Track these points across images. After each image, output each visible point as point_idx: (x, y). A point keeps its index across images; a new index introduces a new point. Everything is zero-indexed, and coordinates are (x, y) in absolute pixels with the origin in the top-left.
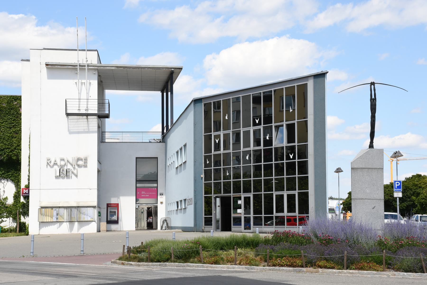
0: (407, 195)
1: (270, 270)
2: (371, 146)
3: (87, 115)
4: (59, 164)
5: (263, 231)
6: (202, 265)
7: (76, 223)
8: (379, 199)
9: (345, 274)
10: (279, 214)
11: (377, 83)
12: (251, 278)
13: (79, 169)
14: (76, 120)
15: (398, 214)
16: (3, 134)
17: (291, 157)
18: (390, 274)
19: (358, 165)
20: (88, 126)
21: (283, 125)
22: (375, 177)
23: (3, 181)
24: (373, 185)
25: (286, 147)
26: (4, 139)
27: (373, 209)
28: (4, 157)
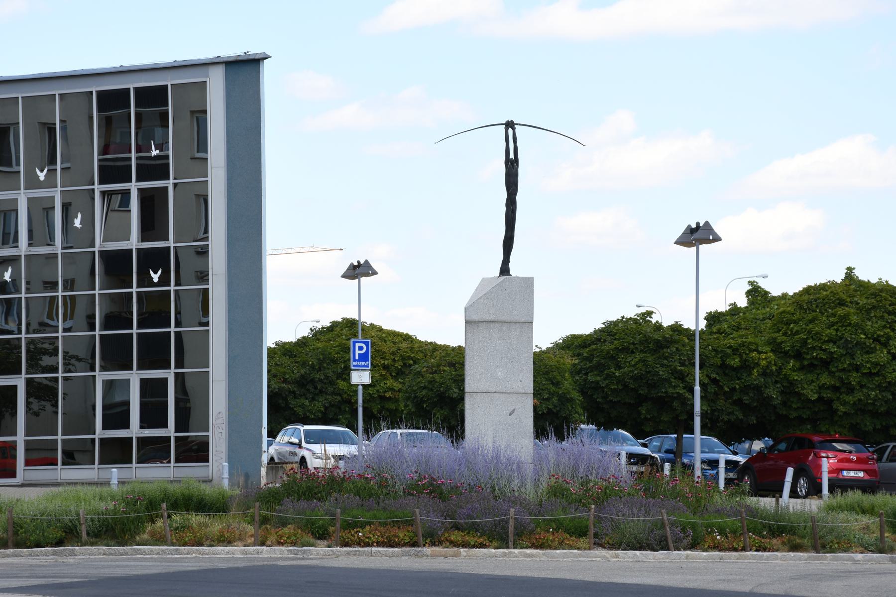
0: (327, 377)
1: (347, 553)
2: (505, 270)
5: (59, 480)
6: (174, 550)
8: (523, 391)
9: (516, 557)
10: (109, 433)
11: (520, 125)
12: (373, 566)
17: (156, 277)
18: (608, 556)
19: (479, 314)
21: (130, 189)
22: (515, 342)
25: (138, 250)
27: (510, 415)
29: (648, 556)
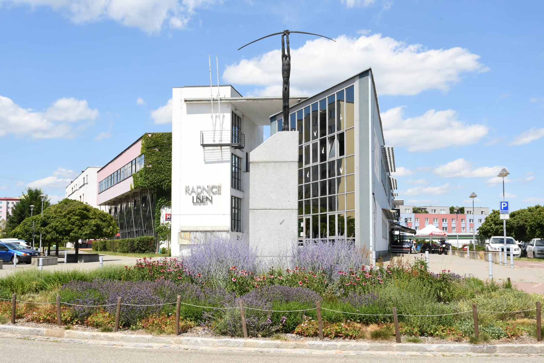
3: (221, 145)
13: (213, 196)
14: (211, 151)
16: (164, 167)
18: (173, 342)
20: (222, 157)
23: (165, 208)
26: (164, 171)
28: (165, 187)
29: (208, 344)
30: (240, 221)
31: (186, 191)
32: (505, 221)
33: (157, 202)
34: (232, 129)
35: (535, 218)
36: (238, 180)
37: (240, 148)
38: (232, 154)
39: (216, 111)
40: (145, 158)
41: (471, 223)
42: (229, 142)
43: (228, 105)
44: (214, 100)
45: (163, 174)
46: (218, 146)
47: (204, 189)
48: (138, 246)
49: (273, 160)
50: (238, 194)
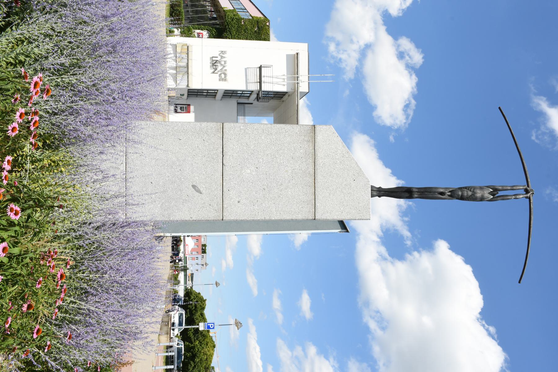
3: (260, 82)
4: (222, 60)
7: (175, 72)
8: (225, 206)
13: (218, 75)
15: (184, 327)
23: (207, 34)
24: (265, 187)
27: (194, 186)
30: (197, 97)
31: (222, 52)
32: (198, 326)
33: (213, 28)
34: (274, 92)
35: (200, 351)
36: (231, 96)
37: (258, 98)
38: (252, 91)
39: (288, 78)
40: (249, 19)
41: (196, 258)
42: (263, 89)
43: (294, 89)
44: (298, 77)
45: (236, 33)
46: (260, 80)
47: (224, 67)
48: (176, 10)
49: (318, 172)
50: (219, 96)
